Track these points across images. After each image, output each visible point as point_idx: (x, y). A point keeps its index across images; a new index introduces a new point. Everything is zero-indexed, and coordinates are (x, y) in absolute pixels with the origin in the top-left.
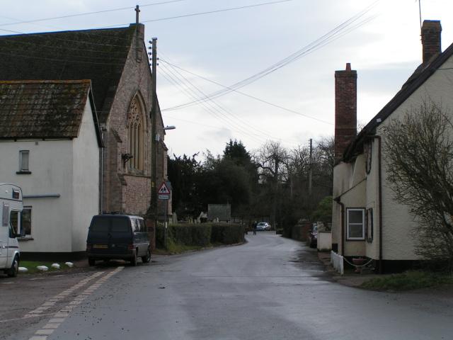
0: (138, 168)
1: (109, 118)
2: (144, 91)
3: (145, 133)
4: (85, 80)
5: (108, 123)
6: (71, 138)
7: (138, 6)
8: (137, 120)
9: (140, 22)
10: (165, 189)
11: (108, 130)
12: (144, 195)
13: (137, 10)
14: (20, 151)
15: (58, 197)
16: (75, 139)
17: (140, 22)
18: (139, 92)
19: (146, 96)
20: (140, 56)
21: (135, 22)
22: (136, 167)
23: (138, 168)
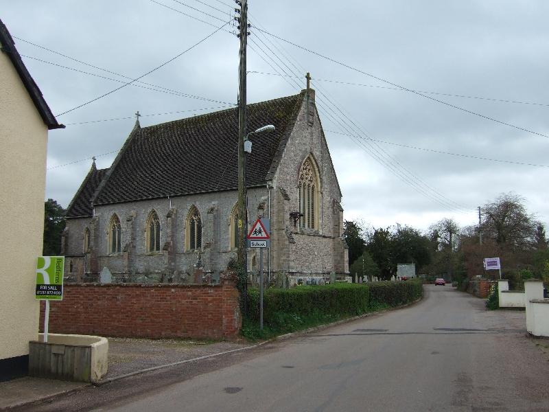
2: (317, 153)
5: (275, 181)
7: (308, 74)
10: (260, 232)
11: (275, 188)
13: (308, 77)
18: (312, 154)
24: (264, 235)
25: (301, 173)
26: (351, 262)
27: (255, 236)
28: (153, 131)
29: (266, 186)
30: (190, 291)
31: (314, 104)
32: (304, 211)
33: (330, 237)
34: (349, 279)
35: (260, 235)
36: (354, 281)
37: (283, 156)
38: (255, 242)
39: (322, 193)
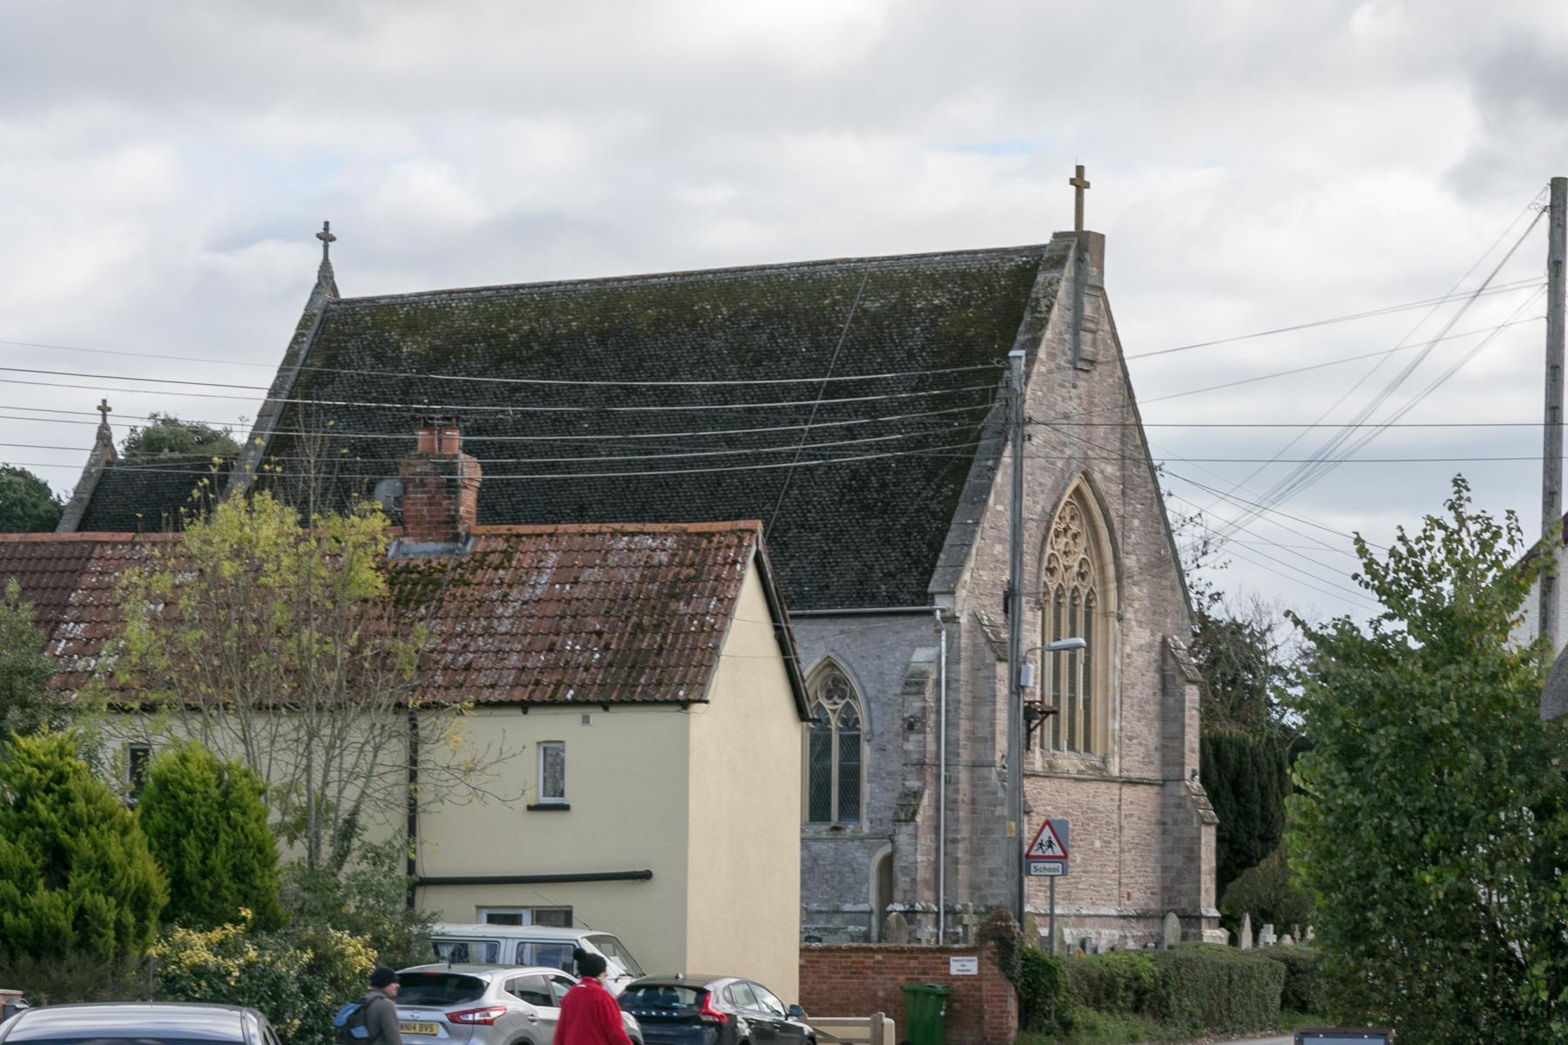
0: (1087, 748)
1: (966, 576)
2: (1106, 471)
3: (1113, 621)
4: (742, 524)
5: (962, 593)
6: (685, 704)
7: (1080, 170)
8: (1082, 575)
9: (1086, 227)
10: (1050, 845)
11: (964, 620)
12: (1106, 843)
13: (1079, 183)
14: (539, 743)
15: (646, 876)
16: (696, 707)
17: (1086, 227)
18: (1087, 476)
19: (1115, 489)
20: (1087, 349)
21: (1070, 227)
22: (1080, 744)
23: (1087, 748)
24: (1058, 851)
25: (1049, 551)
26: (1224, 876)
27: (1040, 853)
28: (382, 311)
29: (931, 613)
30: (916, 958)
31: (1102, 289)
32: (1057, 699)
33: (1150, 783)
34: (1214, 935)
35: (1049, 852)
36: (1234, 940)
37: (991, 501)
38: (1040, 865)
39: (1120, 618)
